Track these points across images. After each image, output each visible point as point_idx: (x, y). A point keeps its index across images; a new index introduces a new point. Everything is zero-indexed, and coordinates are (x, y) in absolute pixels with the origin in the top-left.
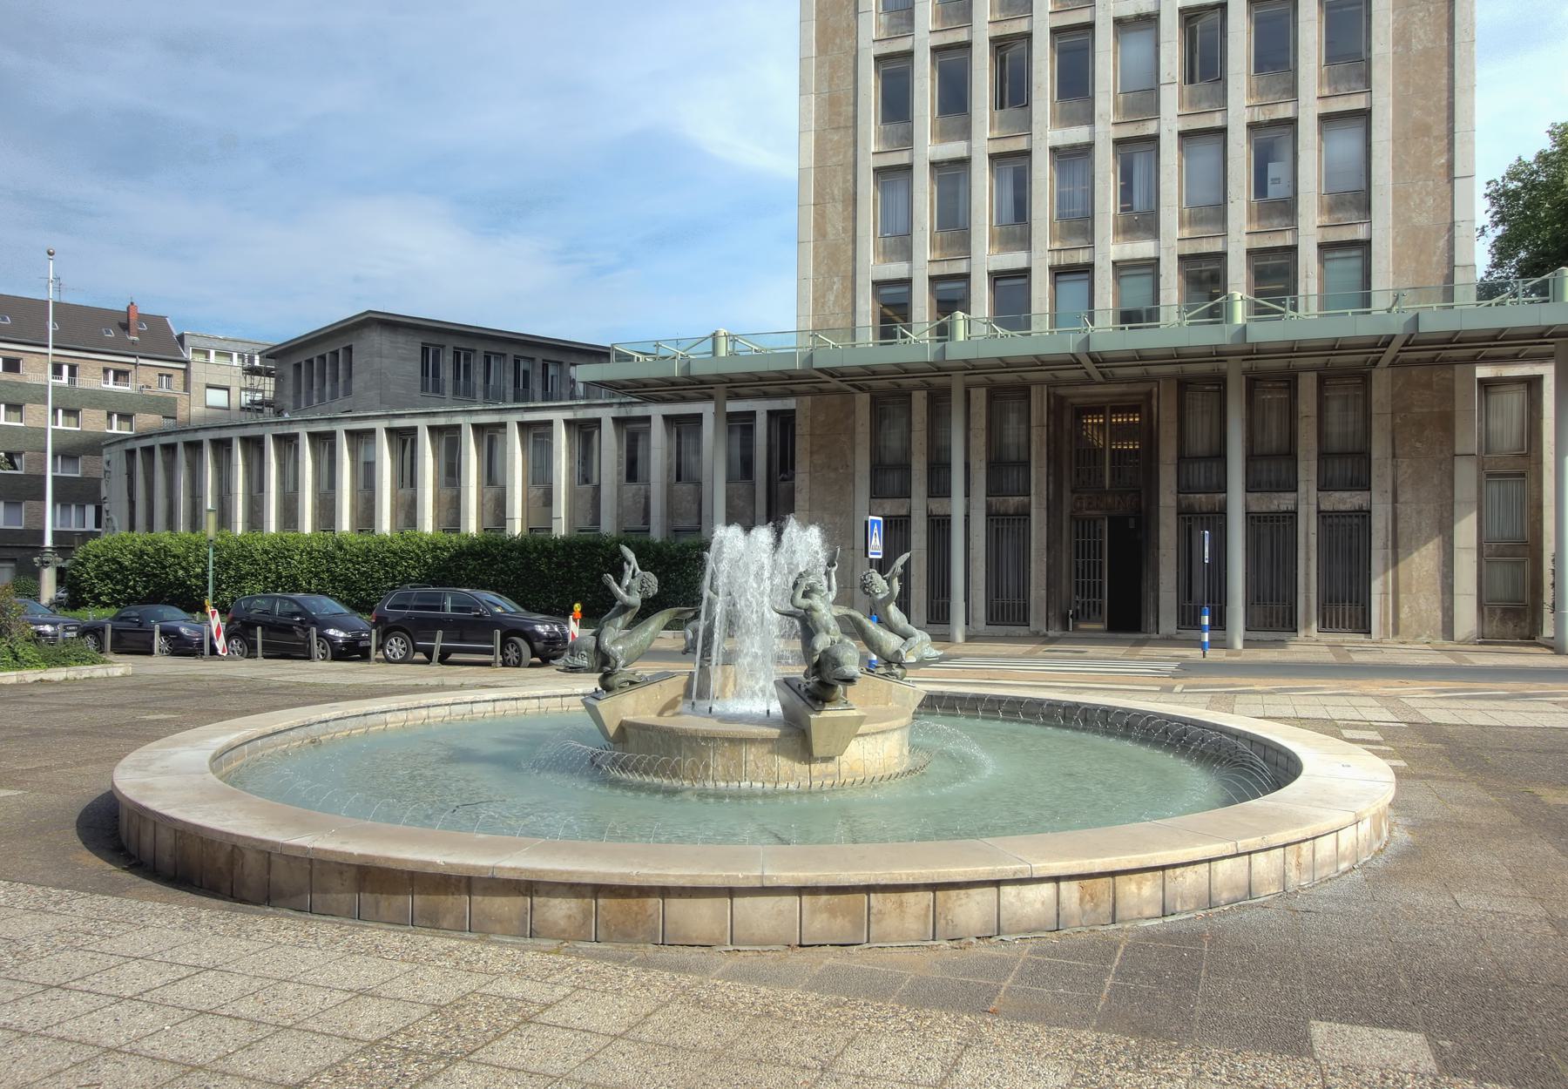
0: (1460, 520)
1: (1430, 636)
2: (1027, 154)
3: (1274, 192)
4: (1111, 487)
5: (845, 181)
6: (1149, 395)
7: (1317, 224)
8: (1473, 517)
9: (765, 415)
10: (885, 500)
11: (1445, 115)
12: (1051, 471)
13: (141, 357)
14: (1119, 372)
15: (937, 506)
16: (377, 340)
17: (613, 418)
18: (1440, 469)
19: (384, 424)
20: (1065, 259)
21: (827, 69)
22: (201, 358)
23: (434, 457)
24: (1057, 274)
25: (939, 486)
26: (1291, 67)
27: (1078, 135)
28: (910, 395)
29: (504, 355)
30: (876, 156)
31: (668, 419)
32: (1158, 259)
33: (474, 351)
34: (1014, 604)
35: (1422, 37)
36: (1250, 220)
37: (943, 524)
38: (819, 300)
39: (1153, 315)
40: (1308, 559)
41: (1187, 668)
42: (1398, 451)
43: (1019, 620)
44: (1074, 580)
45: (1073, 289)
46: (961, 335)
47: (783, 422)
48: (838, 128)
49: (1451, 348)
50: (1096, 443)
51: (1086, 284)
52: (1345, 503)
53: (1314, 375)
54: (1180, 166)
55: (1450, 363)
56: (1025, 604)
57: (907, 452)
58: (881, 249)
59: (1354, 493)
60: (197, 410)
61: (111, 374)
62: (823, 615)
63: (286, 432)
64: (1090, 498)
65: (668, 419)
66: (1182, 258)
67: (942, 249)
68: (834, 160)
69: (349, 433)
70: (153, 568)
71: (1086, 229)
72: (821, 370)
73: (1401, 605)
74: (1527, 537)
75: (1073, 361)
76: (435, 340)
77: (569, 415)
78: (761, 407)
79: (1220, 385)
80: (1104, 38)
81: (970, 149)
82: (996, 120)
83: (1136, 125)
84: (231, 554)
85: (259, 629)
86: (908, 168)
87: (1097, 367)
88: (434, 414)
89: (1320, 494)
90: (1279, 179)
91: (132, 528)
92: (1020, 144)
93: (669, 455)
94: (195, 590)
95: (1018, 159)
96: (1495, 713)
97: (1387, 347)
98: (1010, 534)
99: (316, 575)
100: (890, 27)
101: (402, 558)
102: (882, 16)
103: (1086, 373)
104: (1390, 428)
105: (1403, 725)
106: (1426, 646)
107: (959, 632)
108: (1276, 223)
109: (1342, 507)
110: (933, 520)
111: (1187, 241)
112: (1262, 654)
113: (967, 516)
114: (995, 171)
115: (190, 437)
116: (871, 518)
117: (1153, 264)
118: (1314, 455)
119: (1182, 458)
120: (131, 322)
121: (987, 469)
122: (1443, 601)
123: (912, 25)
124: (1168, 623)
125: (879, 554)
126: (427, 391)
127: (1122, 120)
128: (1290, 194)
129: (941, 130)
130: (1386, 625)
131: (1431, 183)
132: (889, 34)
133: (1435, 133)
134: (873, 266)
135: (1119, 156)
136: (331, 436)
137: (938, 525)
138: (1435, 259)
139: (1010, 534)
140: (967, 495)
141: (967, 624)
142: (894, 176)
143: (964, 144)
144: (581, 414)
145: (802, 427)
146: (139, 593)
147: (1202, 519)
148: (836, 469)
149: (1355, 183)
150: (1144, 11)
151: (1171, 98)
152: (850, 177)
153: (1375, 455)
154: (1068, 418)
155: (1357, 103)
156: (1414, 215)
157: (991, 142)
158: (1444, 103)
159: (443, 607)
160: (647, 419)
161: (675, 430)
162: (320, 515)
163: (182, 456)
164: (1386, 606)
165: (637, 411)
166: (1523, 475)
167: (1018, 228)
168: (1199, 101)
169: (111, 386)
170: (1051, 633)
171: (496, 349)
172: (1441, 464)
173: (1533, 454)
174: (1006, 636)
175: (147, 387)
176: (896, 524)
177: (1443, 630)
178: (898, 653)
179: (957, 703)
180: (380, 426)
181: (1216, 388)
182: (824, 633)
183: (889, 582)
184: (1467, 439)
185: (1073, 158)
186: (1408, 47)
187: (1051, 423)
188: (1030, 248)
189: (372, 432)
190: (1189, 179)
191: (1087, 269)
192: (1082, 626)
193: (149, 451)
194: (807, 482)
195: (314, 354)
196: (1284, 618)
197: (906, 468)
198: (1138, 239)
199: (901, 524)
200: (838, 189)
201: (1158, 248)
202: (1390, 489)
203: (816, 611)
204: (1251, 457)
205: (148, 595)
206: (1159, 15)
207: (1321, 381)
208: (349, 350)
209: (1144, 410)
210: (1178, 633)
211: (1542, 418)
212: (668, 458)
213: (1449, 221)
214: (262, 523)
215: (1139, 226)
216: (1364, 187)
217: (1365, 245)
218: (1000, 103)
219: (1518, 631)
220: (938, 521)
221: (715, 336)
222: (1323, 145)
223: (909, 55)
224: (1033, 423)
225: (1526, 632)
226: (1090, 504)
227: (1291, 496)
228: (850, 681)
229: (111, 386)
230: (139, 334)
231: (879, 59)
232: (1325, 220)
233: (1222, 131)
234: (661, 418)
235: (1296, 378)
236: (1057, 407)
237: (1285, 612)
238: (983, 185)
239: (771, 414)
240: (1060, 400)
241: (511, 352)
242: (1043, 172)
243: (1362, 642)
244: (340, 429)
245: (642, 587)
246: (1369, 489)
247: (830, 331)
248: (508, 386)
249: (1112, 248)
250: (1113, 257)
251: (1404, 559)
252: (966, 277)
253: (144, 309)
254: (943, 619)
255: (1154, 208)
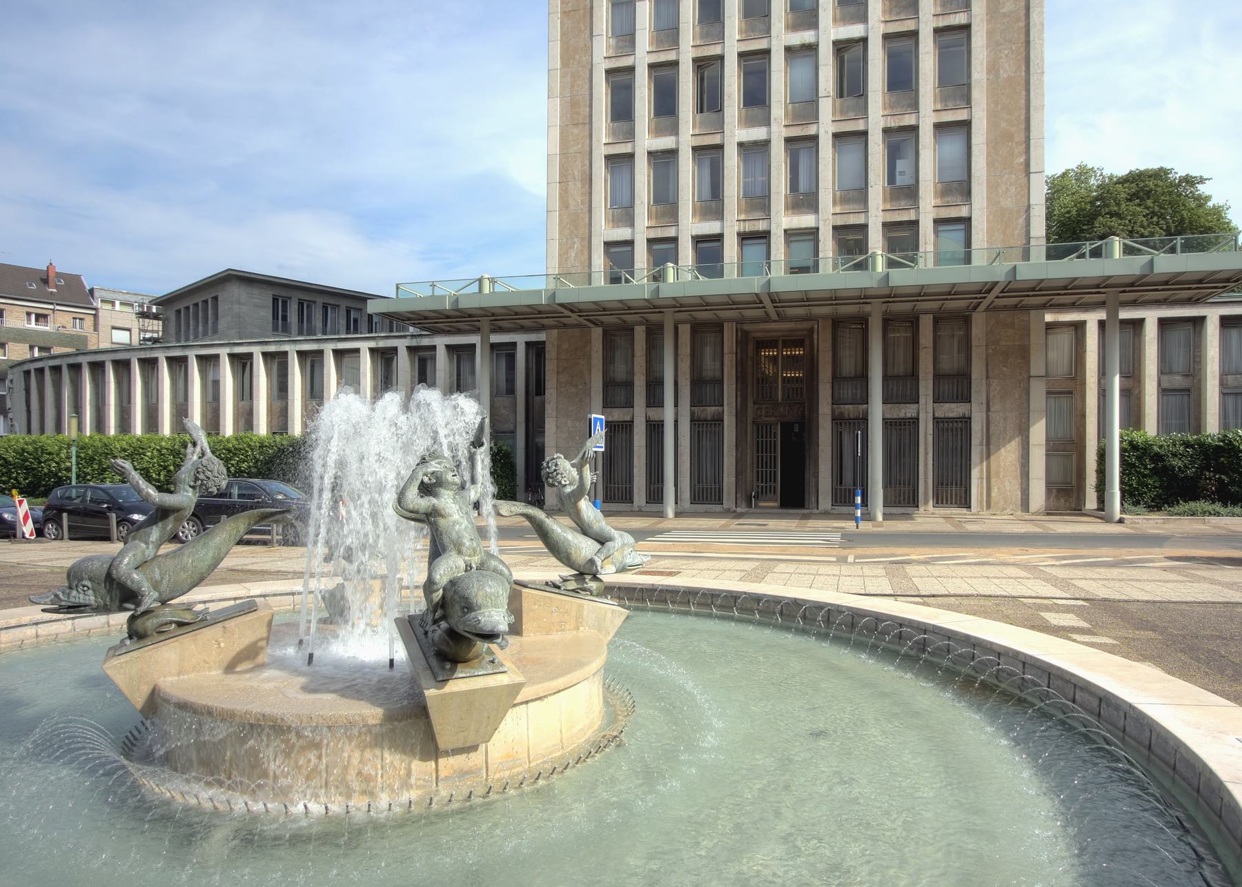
0: (1034, 424)
1: (1012, 510)
2: (720, 147)
3: (899, 181)
4: (782, 400)
5: (583, 165)
6: (811, 331)
7: (933, 204)
8: (1043, 422)
9: (524, 345)
10: (614, 409)
11: (1023, 126)
12: (739, 387)
13: (57, 304)
14: (791, 312)
15: (654, 414)
16: (235, 291)
17: (407, 347)
18: (1020, 387)
19: (227, 350)
20: (749, 227)
21: (568, 79)
22: (109, 307)
23: (267, 376)
24: (743, 239)
25: (655, 399)
26: (914, 88)
27: (758, 133)
28: (633, 329)
29: (338, 306)
30: (606, 146)
31: (449, 348)
32: (817, 229)
33: (315, 302)
34: (711, 488)
35: (1007, 68)
36: (885, 201)
37: (658, 428)
38: (563, 256)
39: (816, 268)
40: (926, 454)
41: (850, 540)
42: (991, 374)
43: (715, 500)
44: (755, 469)
45: (755, 250)
46: (671, 277)
47: (537, 349)
48: (577, 124)
49: (1033, 296)
50: (767, 372)
51: (764, 247)
52: (953, 412)
53: (931, 316)
54: (834, 160)
55: (1028, 308)
56: (719, 488)
57: (631, 372)
58: (611, 218)
59: (959, 405)
60: (104, 345)
61: (33, 316)
62: (455, 523)
63: (148, 356)
64: (767, 408)
65: (449, 348)
66: (835, 228)
67: (656, 218)
68: (575, 148)
69: (199, 357)
70: (31, 463)
71: (765, 204)
72: (562, 305)
73: (992, 486)
74: (1074, 437)
75: (757, 300)
76: (284, 293)
77: (373, 344)
78: (520, 339)
79: (862, 324)
80: (778, 61)
81: (678, 142)
82: (698, 122)
83: (801, 127)
84: (95, 452)
85: (65, 515)
86: (631, 156)
87: (775, 307)
88: (266, 343)
89: (935, 405)
90: (904, 172)
91: (29, 431)
92: (715, 140)
93: (451, 376)
94: (65, 480)
95: (713, 151)
96: (1153, 585)
97: (989, 293)
98: (708, 435)
99: (165, 468)
100: (618, 47)
101: (235, 454)
102: (611, 40)
103: (765, 312)
104: (984, 357)
105: (1080, 603)
106: (1011, 517)
107: (670, 511)
108: (903, 204)
109: (951, 415)
110: (650, 425)
111: (839, 216)
112: (899, 525)
113: (676, 421)
114: (697, 160)
115: (72, 361)
116: (594, 416)
117: (813, 233)
118: (931, 376)
119: (836, 378)
120: (50, 278)
121: (691, 385)
122: (1021, 483)
123: (634, 47)
124: (825, 502)
125: (602, 447)
126: (277, 331)
127: (791, 123)
128: (913, 182)
129: (656, 129)
130: (981, 502)
131: (1013, 176)
132: (616, 53)
133: (1016, 140)
134: (604, 230)
135: (789, 151)
136: (183, 360)
137: (655, 428)
138: (1016, 232)
139: (708, 435)
140: (676, 405)
141: (676, 503)
142: (620, 162)
143: (673, 138)
144: (382, 344)
145: (551, 353)
146: (21, 483)
147: (850, 423)
148: (576, 386)
149: (959, 175)
150: (807, 42)
151: (826, 107)
152: (587, 162)
153: (973, 377)
154: (751, 347)
155: (961, 115)
156: (1001, 199)
157: (693, 137)
158: (1023, 117)
159: (230, 494)
160: (434, 348)
161: (455, 356)
162: (177, 422)
163: (66, 376)
164: (982, 487)
165: (426, 342)
166: (1071, 393)
167: (713, 204)
168: (847, 111)
169: (33, 325)
170: (739, 510)
171: (331, 301)
172: (1020, 383)
173: (1078, 378)
174: (706, 512)
175: (63, 327)
176: (622, 428)
177: (1022, 505)
178: (592, 562)
179: (668, 596)
180: (223, 352)
181: (859, 326)
182: (453, 553)
183: (580, 468)
184: (1037, 367)
185: (755, 151)
186: (997, 75)
187: (739, 351)
188: (723, 219)
189: (217, 357)
190: (839, 172)
191: (765, 236)
192: (761, 504)
193: (40, 371)
194: (555, 395)
195: (190, 302)
196: (909, 497)
197: (629, 385)
198: (803, 213)
199: (626, 428)
200: (577, 170)
201: (817, 220)
202: (984, 402)
203: (442, 516)
204: (886, 378)
205: (29, 484)
206: (818, 45)
207: (936, 321)
208: (215, 299)
209: (807, 342)
210: (832, 509)
211: (1085, 351)
212: (450, 378)
213: (1026, 204)
214: (157, 426)
215: (803, 204)
216: (966, 178)
217: (967, 221)
218: (700, 109)
219: (1068, 505)
220: (654, 425)
221: (480, 281)
222: (937, 146)
223: (631, 70)
224: (726, 351)
225: (1073, 506)
226: (767, 412)
227: (914, 406)
228: (490, 636)
229: (33, 325)
230: (57, 287)
231: (609, 72)
232: (938, 202)
233: (864, 134)
234: (444, 347)
235: (918, 319)
236: (743, 339)
237: (909, 493)
238: (687, 169)
239: (528, 344)
240: (746, 334)
241: (344, 304)
242: (732, 160)
243: (965, 514)
244: (192, 355)
245: (196, 479)
246: (970, 402)
247: (567, 275)
248: (341, 329)
249: (784, 219)
250: (785, 226)
251: (994, 453)
252: (675, 240)
253: (60, 268)
254: (658, 499)
255: (815, 190)
